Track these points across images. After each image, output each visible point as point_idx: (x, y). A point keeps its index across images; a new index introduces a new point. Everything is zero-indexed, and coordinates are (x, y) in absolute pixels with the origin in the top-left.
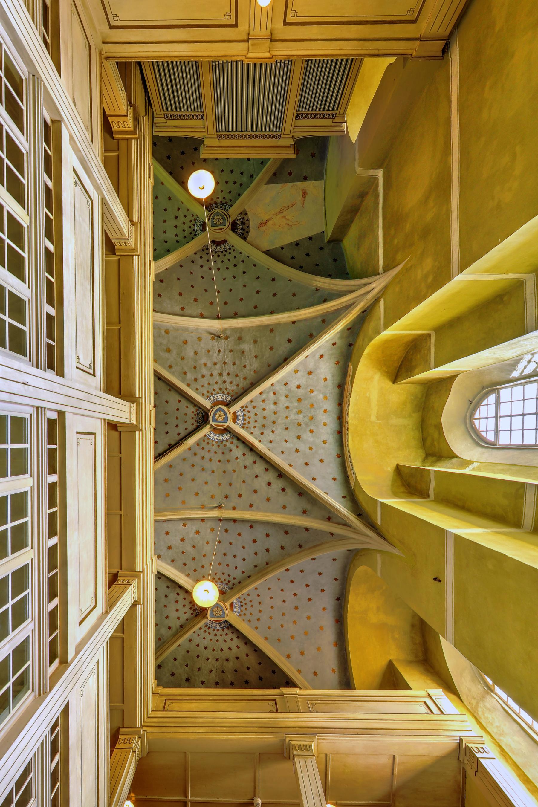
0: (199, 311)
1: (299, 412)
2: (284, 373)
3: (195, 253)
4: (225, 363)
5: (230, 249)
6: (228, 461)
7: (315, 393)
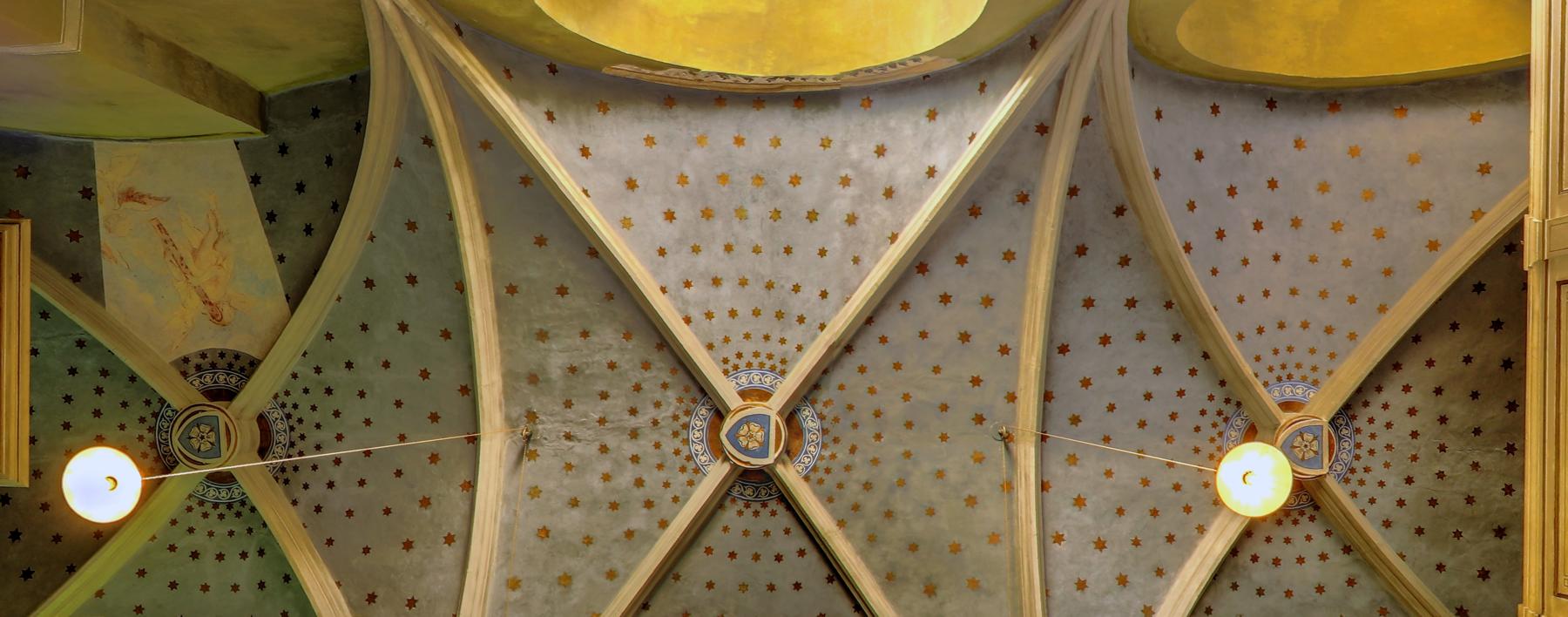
1: (741, 214)
3: (295, 503)
4: (602, 421)
5: (283, 406)
6: (878, 414)
7: (687, 170)
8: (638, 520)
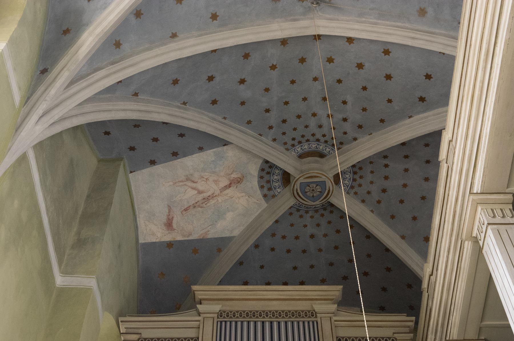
3: (355, 139)
5: (293, 145)
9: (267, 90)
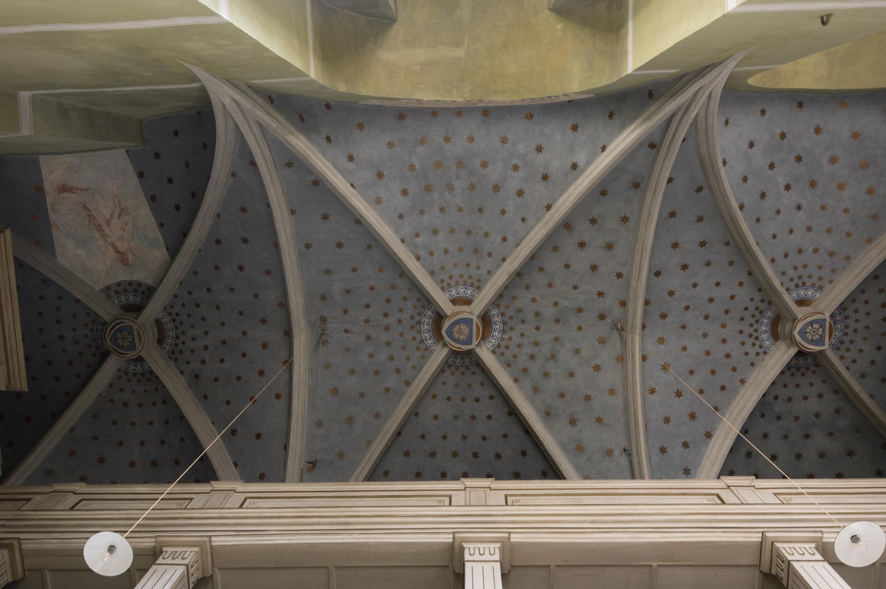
0: (282, 369)
1: (450, 187)
2: (383, 224)
3: (182, 373)
4: (367, 321)
6: (537, 314)
7: (415, 161)
8: (392, 381)
9: (232, 290)
